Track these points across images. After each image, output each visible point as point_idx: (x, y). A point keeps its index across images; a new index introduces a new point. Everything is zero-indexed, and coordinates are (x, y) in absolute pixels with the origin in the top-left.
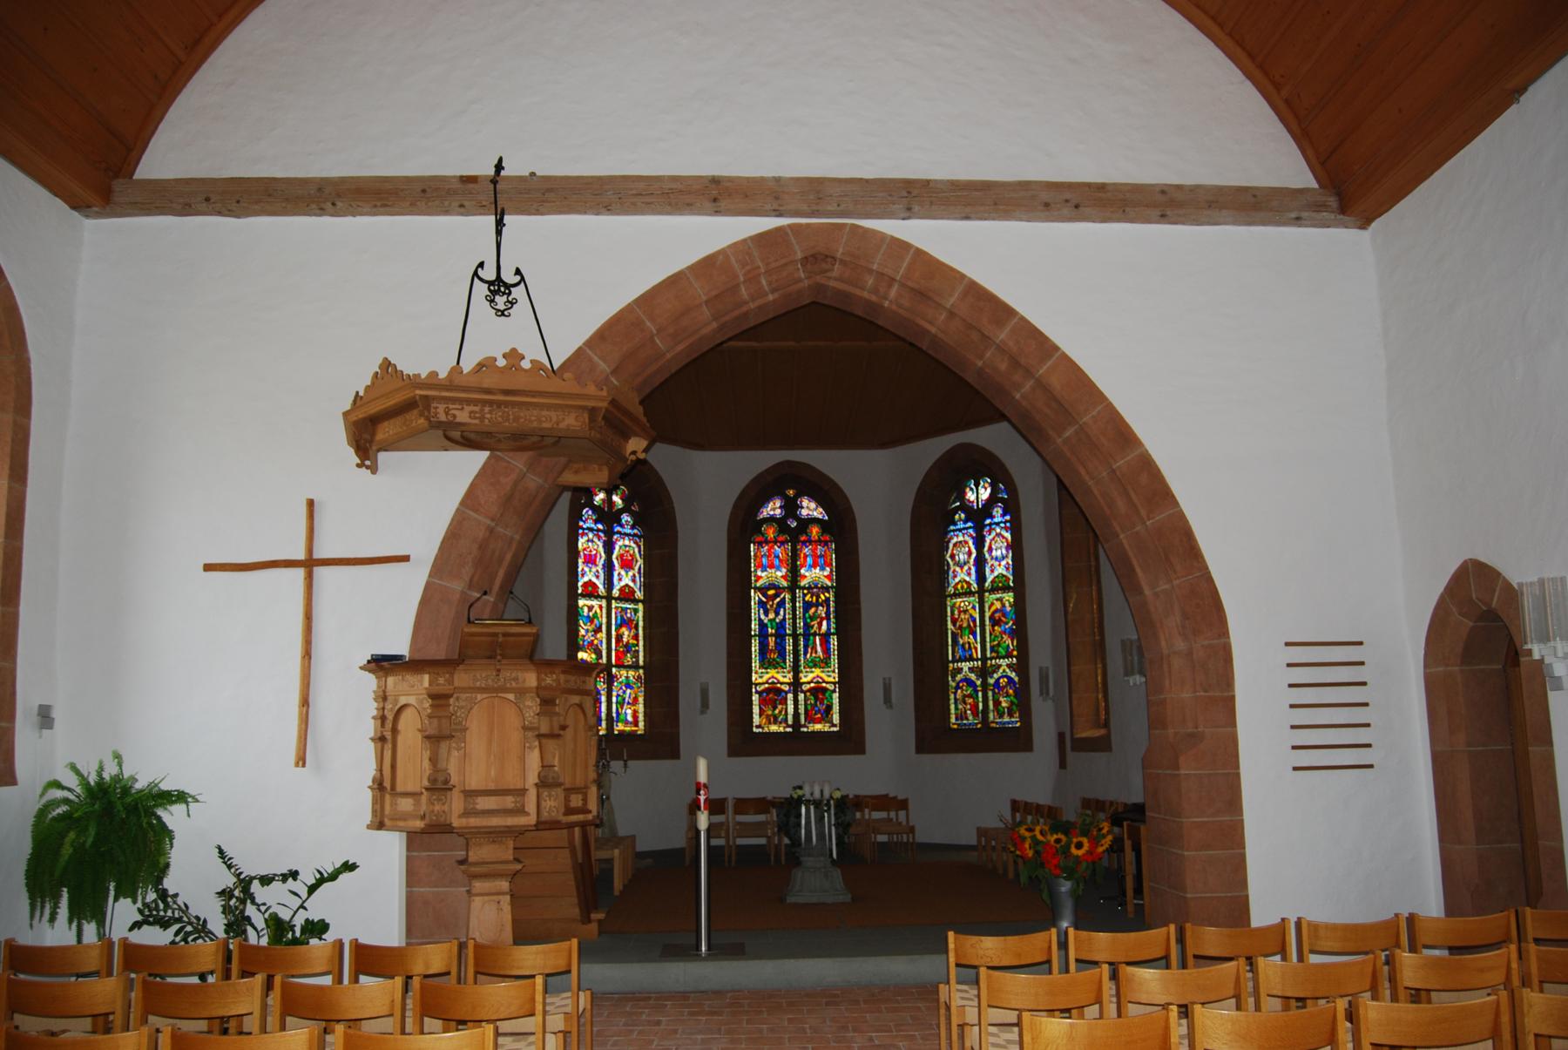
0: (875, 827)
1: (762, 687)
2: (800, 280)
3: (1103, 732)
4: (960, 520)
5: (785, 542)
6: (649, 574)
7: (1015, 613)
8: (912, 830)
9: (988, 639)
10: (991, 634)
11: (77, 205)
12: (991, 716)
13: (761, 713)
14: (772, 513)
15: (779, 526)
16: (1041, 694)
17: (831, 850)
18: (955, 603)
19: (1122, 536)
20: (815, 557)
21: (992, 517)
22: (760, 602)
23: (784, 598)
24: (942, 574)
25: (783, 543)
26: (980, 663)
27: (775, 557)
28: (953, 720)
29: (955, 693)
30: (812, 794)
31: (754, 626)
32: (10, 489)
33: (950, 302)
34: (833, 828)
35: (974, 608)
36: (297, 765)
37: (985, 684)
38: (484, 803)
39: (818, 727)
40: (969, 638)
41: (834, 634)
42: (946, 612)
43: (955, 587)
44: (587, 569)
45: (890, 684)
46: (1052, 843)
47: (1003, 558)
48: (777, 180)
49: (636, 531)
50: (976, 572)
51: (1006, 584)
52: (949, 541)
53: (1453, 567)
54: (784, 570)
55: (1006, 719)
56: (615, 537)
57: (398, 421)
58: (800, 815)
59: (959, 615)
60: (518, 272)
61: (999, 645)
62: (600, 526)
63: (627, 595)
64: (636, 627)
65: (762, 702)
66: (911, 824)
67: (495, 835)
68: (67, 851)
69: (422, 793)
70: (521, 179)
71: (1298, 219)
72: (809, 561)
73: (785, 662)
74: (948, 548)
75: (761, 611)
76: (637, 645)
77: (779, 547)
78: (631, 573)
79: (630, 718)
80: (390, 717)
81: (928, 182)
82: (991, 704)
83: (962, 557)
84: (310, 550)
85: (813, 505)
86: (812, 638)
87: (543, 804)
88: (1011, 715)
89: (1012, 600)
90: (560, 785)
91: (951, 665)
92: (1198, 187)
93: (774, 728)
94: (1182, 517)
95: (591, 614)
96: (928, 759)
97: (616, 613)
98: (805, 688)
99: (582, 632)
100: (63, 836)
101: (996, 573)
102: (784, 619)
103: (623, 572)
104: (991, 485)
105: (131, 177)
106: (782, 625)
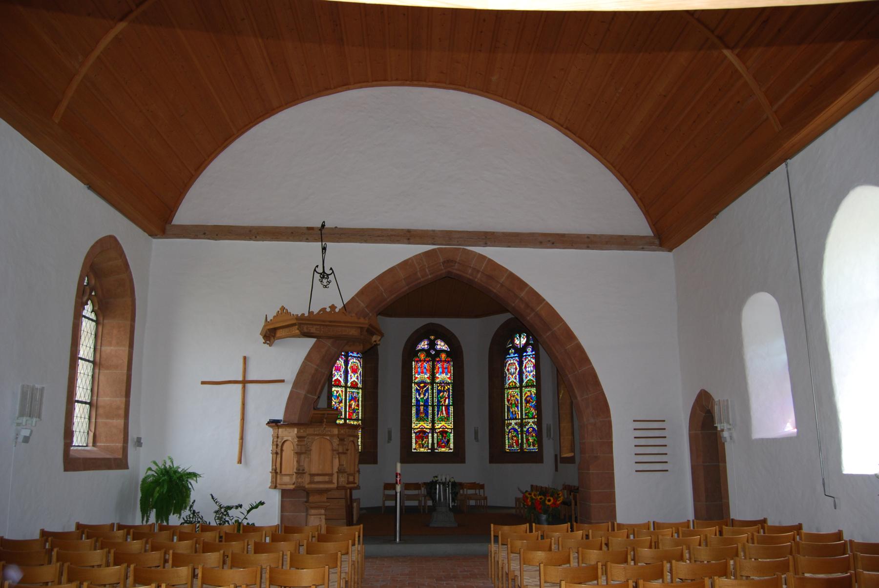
0: (469, 497)
1: (417, 430)
2: (442, 270)
3: (573, 454)
4: (512, 353)
5: (429, 361)
6: (365, 375)
7: (536, 398)
8: (486, 498)
9: (524, 410)
10: (525, 407)
11: (152, 235)
13: (416, 442)
14: (423, 347)
15: (426, 353)
16: (547, 436)
17: (449, 504)
18: (509, 393)
19: (569, 376)
20: (443, 368)
21: (527, 352)
22: (417, 389)
23: (428, 388)
24: (503, 378)
25: (428, 361)
28: (507, 447)
29: (508, 435)
30: (441, 480)
31: (414, 401)
32: (129, 351)
33: (502, 280)
34: (450, 494)
35: (517, 394)
36: (238, 463)
37: (522, 431)
38: (317, 479)
39: (443, 450)
41: (451, 405)
42: (505, 396)
43: (509, 384)
44: (336, 373)
45: (477, 430)
46: (539, 499)
47: (532, 371)
48: (434, 231)
49: (359, 355)
50: (519, 378)
51: (532, 384)
52: (507, 363)
53: (697, 392)
54: (428, 374)
55: (532, 447)
56: (349, 358)
57: (287, 330)
58: (436, 489)
60: (331, 269)
61: (529, 412)
63: (354, 386)
65: (417, 437)
66: (486, 495)
67: (321, 492)
68: (156, 495)
69: (293, 475)
70: (332, 229)
71: (643, 248)
72: (440, 370)
73: (428, 418)
74: (506, 366)
75: (417, 394)
76: (359, 409)
77: (426, 363)
78: (356, 375)
80: (280, 444)
81: (494, 232)
82: (525, 440)
83: (513, 370)
84: (244, 376)
85: (443, 344)
86: (441, 407)
87: (340, 480)
88: (534, 446)
89: (535, 391)
90: (346, 472)
91: (506, 421)
92: (602, 235)
93: (422, 450)
94: (593, 368)
95: (337, 394)
96: (494, 465)
98: (437, 431)
99: (333, 403)
100: (154, 488)
101: (528, 379)
102: (428, 398)
103: (353, 375)
104: (527, 337)
105: (170, 223)
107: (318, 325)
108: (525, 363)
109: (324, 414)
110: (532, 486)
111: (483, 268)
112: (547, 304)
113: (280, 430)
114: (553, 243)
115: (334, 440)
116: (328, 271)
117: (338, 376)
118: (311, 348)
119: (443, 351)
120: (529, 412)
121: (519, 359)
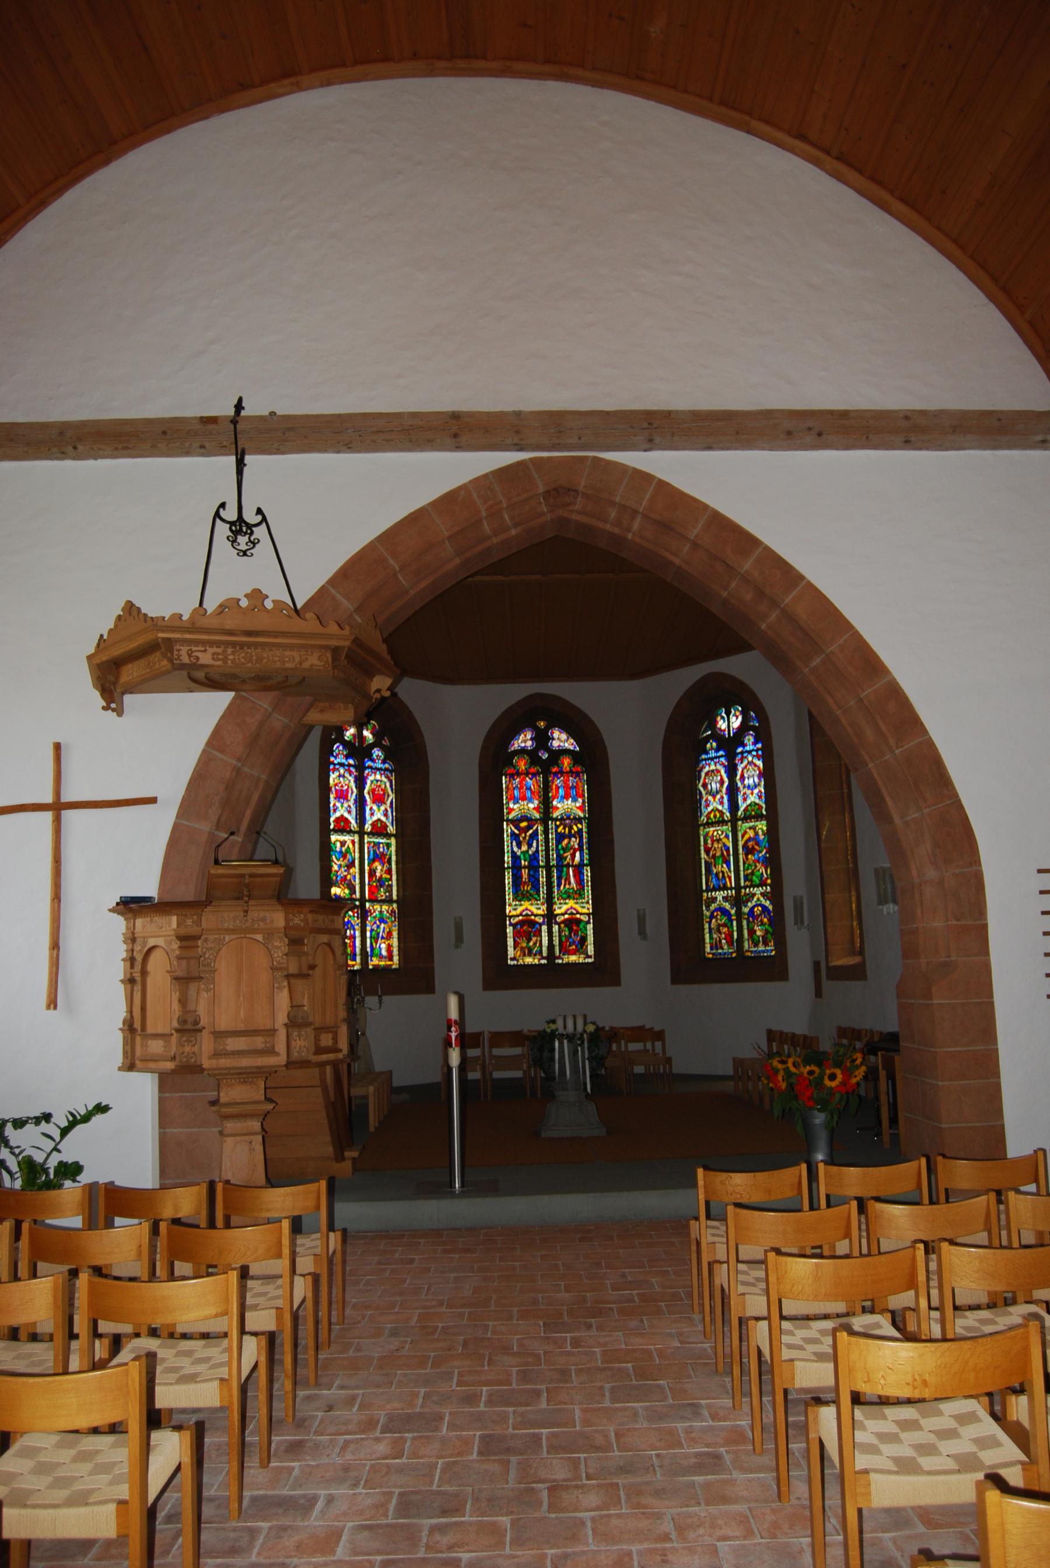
1: (517, 919)
4: (712, 748)
7: (769, 841)
8: (669, 1060)
9: (742, 868)
10: (744, 863)
12: (746, 945)
13: (516, 945)
14: (523, 745)
16: (796, 923)
17: (585, 1084)
18: (707, 834)
19: (870, 765)
20: (567, 788)
21: (744, 745)
22: (513, 834)
23: (537, 829)
24: (694, 803)
25: (534, 775)
26: (734, 892)
27: (527, 788)
28: (708, 949)
29: (710, 923)
31: (507, 858)
33: (694, 532)
35: (727, 837)
36: (48, 1007)
37: (739, 913)
38: (234, 1044)
39: (573, 958)
40: (722, 867)
41: (587, 865)
42: (699, 842)
44: (338, 805)
45: (644, 914)
46: (805, 1074)
47: (756, 786)
48: (518, 414)
49: (387, 766)
51: (758, 812)
52: (701, 770)
54: (536, 802)
55: (761, 948)
56: (366, 772)
57: (142, 663)
58: (554, 1049)
59: (712, 844)
60: (259, 511)
61: (752, 874)
62: (351, 762)
63: (379, 830)
64: (389, 862)
65: (516, 934)
66: (668, 1055)
69: (172, 1035)
70: (261, 418)
72: (561, 792)
75: (514, 843)
76: (391, 879)
77: (531, 779)
78: (383, 808)
79: (384, 953)
80: (139, 958)
82: (746, 932)
85: (564, 736)
86: (565, 869)
87: (293, 1044)
91: (705, 894)
93: (529, 960)
94: (930, 744)
95: (344, 849)
96: (684, 989)
97: (368, 848)
98: (559, 919)
99: (335, 867)
101: (748, 802)
103: (375, 807)
104: (742, 713)
106: (534, 857)
107: (217, 643)
108: (740, 768)
109: (242, 876)
110: (770, 1032)
111: (644, 503)
112: (810, 586)
113: (139, 922)
114: (820, 434)
115: (277, 944)
116: (251, 517)
117: (342, 810)
118: (223, 717)
119: (567, 752)
120: (752, 874)
121: (727, 760)
